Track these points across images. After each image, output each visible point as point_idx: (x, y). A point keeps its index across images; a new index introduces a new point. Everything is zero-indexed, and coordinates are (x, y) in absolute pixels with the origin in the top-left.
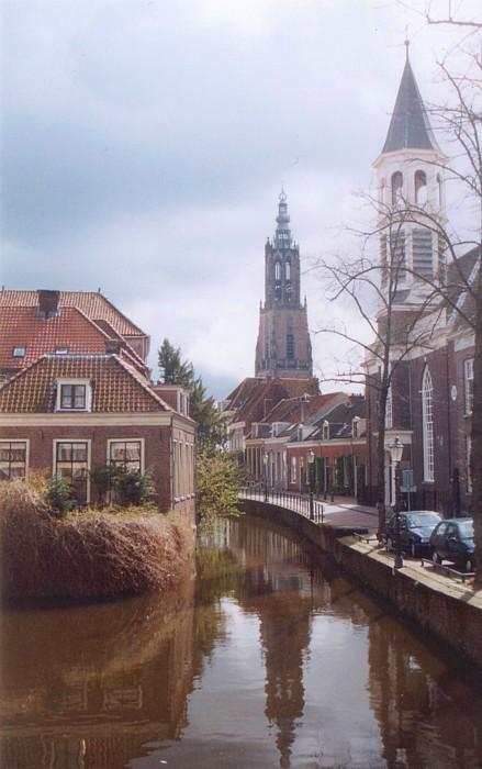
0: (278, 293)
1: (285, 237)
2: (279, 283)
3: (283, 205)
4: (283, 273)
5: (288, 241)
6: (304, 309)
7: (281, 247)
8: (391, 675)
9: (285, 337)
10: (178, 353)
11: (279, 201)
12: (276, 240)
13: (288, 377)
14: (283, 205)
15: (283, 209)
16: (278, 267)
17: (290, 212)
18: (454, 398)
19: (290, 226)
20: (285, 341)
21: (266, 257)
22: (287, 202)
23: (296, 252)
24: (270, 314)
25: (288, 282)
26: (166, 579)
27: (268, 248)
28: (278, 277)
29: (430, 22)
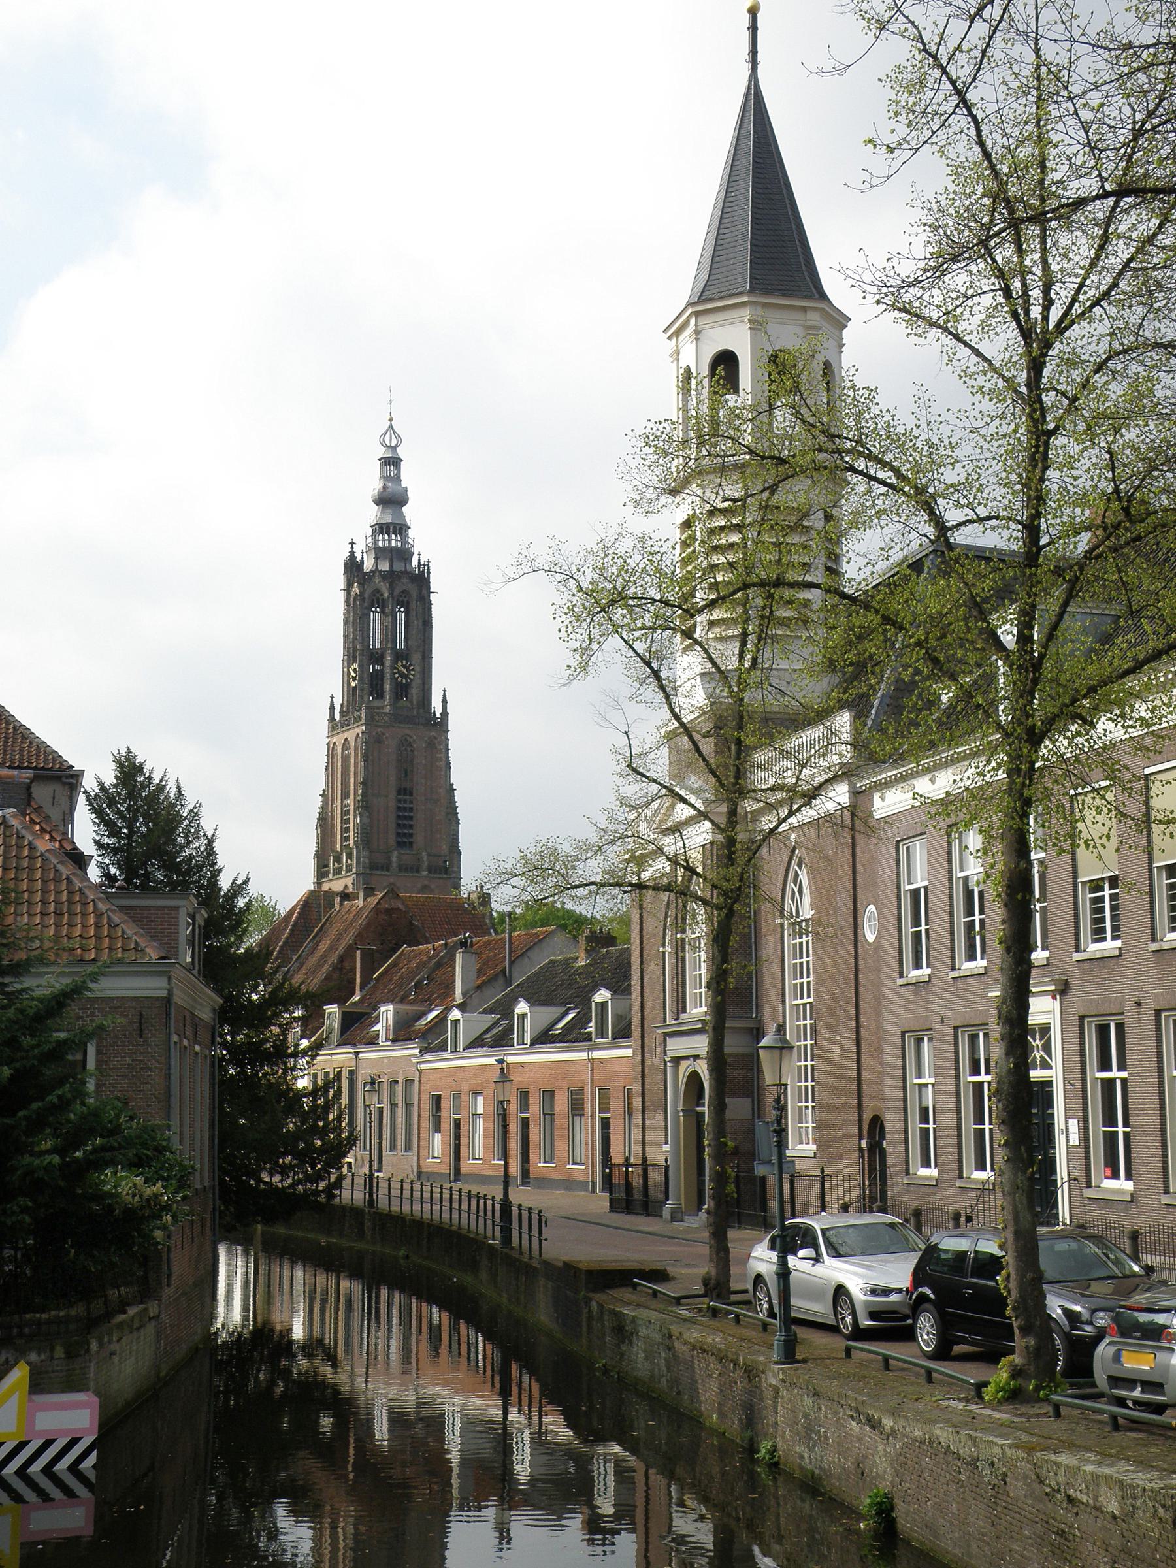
0: (374, 684)
3: (392, 462)
4: (389, 633)
5: (404, 554)
6: (441, 725)
7: (384, 566)
8: (518, 1467)
9: (393, 795)
10: (220, 870)
11: (381, 452)
13: (411, 892)
14: (392, 462)
16: (375, 618)
17: (409, 477)
18: (871, 937)
20: (392, 804)
21: (348, 589)
22: (401, 452)
23: (421, 580)
24: (354, 733)
25: (398, 656)
26: (168, 814)
27: (352, 567)
28: (375, 643)
29: (903, 1033)
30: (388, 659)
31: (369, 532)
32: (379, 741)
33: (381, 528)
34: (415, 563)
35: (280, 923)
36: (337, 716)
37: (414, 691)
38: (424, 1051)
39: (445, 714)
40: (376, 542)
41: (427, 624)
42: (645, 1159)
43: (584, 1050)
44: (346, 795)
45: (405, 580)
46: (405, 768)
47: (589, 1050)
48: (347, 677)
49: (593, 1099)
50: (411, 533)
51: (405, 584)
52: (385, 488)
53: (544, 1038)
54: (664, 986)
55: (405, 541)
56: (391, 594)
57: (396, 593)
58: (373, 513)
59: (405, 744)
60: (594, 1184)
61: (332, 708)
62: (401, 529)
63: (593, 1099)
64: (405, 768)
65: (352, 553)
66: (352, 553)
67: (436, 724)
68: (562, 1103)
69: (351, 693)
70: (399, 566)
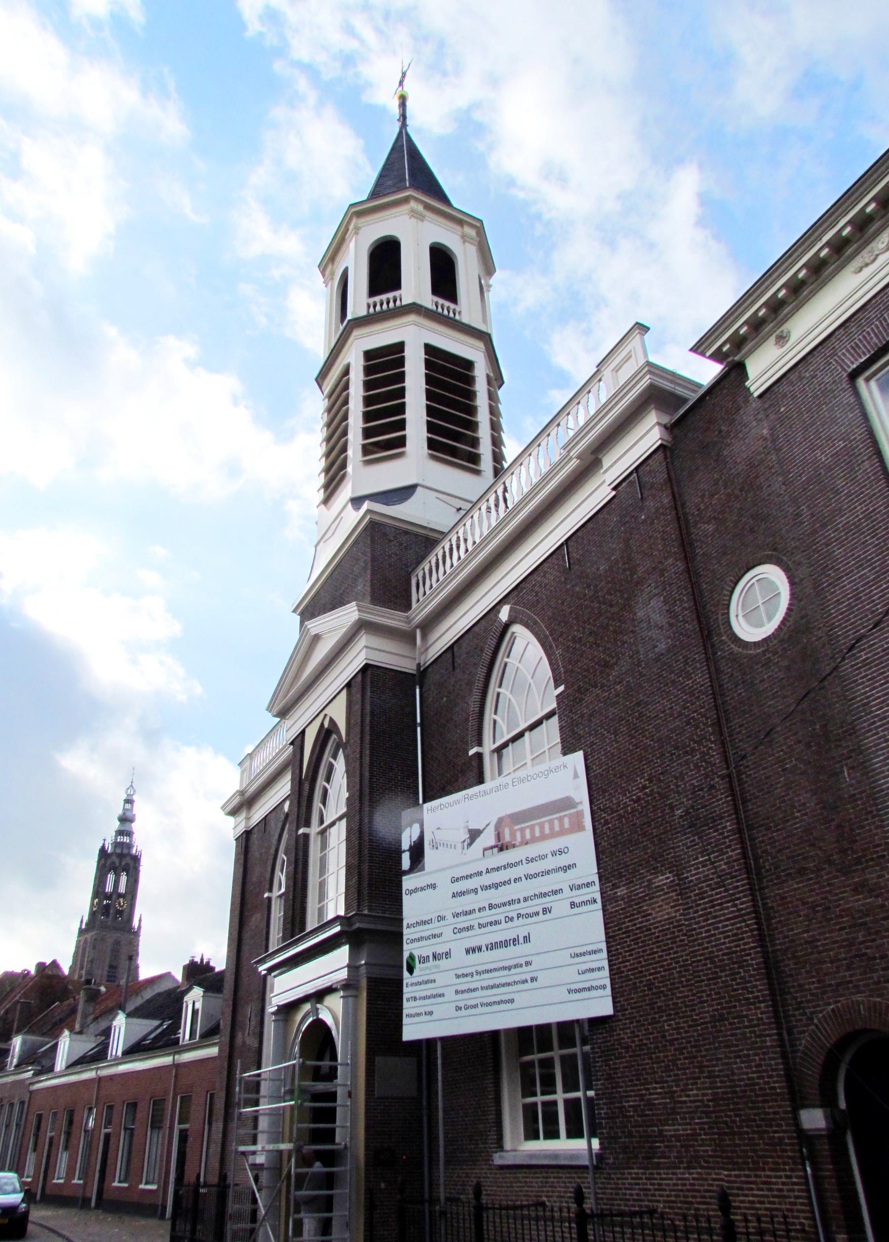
1: (126, 839)
2: (109, 897)
3: (129, 801)
5: (130, 846)
6: (137, 934)
7: (118, 851)
9: (107, 968)
12: (116, 844)
14: (129, 801)
15: (128, 806)
19: (135, 826)
20: (105, 973)
23: (136, 859)
25: (120, 895)
27: (103, 851)
30: (114, 897)
31: (114, 834)
32: (103, 939)
33: (120, 833)
34: (134, 851)
35: (24, 1027)
36: (84, 926)
37: (125, 914)
38: (37, 1074)
39: (139, 927)
40: (116, 839)
41: (136, 881)
42: (223, 1177)
43: (169, 1054)
44: (82, 968)
45: (128, 858)
46: (115, 952)
47: (175, 1053)
48: (92, 905)
49: (174, 1107)
50: (135, 836)
51: (128, 860)
52: (124, 814)
53: (135, 1050)
54: (201, 1158)
55: (131, 841)
56: (120, 863)
57: (123, 863)
58: (117, 825)
59: (117, 943)
60: (164, 1207)
61: (82, 922)
62: (129, 834)
63: (174, 1107)
64: (115, 952)
65: (104, 845)
66: (104, 845)
67: (134, 932)
68: (144, 1112)
69: (93, 914)
70: (125, 851)
